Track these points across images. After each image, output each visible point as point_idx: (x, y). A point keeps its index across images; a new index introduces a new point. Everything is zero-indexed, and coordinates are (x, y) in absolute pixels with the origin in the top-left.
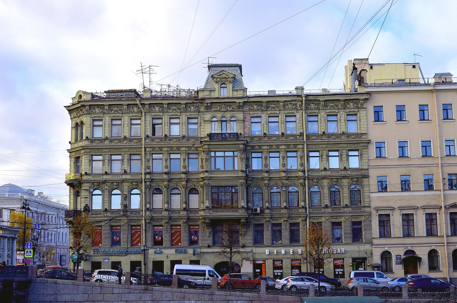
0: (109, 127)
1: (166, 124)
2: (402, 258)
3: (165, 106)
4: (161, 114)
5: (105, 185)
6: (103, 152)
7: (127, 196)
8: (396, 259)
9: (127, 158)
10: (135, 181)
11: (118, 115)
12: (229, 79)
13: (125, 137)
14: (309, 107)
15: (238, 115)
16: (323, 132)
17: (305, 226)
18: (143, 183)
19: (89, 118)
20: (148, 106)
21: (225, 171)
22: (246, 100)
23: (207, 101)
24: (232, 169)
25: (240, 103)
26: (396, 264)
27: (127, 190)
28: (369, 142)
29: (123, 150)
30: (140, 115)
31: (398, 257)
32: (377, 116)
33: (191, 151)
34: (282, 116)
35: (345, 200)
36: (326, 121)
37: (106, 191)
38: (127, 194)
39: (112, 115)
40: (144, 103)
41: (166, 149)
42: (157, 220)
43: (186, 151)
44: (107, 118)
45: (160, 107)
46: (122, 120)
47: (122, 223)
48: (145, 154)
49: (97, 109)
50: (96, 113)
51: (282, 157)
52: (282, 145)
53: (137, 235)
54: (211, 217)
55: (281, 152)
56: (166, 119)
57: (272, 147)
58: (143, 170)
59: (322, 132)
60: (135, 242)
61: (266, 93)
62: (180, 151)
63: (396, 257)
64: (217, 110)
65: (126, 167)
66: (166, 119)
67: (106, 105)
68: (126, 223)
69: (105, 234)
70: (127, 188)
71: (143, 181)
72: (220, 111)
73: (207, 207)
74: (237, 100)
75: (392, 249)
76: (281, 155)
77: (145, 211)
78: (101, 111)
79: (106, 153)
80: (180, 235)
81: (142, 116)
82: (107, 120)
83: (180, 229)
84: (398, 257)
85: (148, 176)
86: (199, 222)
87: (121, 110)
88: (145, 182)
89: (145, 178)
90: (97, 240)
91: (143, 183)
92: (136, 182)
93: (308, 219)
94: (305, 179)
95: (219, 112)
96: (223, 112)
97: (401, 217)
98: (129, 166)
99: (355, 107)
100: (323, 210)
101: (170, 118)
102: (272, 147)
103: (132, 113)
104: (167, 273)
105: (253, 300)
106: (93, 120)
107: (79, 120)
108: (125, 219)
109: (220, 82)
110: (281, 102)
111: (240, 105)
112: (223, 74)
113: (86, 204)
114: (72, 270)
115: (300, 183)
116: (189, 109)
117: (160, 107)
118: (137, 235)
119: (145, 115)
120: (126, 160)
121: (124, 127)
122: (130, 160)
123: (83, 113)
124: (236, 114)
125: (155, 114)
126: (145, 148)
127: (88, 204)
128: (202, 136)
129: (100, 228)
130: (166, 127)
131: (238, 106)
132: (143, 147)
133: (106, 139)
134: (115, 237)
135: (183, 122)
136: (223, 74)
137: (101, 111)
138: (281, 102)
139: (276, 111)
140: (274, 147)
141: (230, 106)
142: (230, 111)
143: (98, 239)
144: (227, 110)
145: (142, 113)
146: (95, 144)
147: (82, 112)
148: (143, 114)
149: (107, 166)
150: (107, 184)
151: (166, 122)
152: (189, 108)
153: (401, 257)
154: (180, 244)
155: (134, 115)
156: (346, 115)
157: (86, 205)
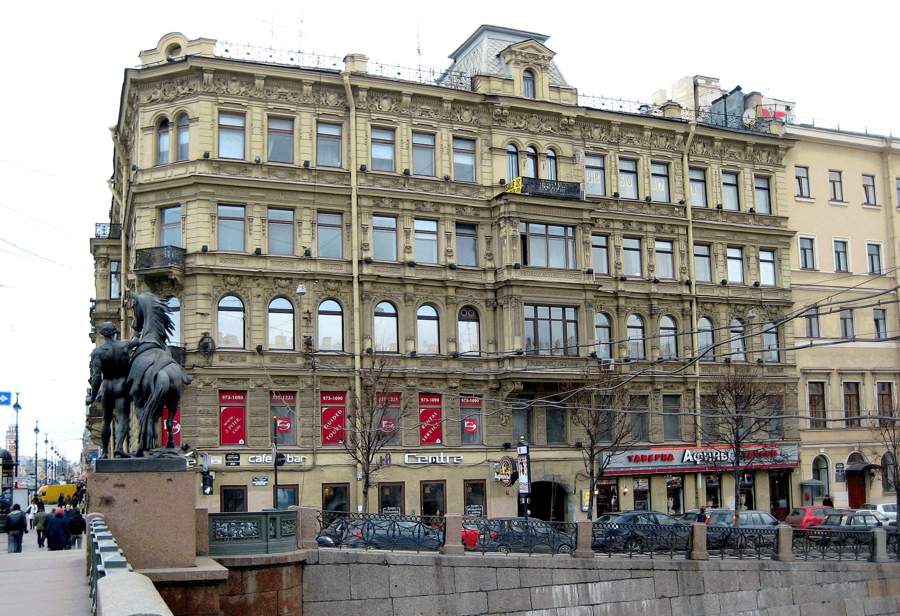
2: (845, 469)
3: (363, 94)
5: (255, 284)
6: (248, 199)
8: (837, 471)
9: (308, 218)
10: (334, 279)
11: (286, 106)
13: (307, 164)
14: (758, 157)
15: (561, 145)
16: (305, 161)
17: (692, 403)
18: (356, 285)
19: (209, 104)
21: (547, 270)
22: (582, 114)
23: (504, 103)
24: (544, 265)
25: (568, 118)
26: (837, 481)
28: (790, 235)
29: (302, 198)
30: (341, 113)
31: (839, 465)
33: (421, 211)
34: (445, 136)
36: (217, 126)
37: (255, 299)
39: (271, 105)
41: (407, 206)
42: (428, 382)
44: (304, 115)
45: (393, 102)
46: (248, 116)
48: (359, 214)
50: (380, 111)
51: (484, 238)
52: (650, 223)
53: (334, 418)
54: (529, 377)
55: (483, 227)
57: (382, 202)
58: (355, 253)
59: (303, 163)
60: (331, 435)
61: (635, 110)
63: (837, 468)
64: (519, 128)
67: (259, 78)
69: (255, 414)
71: (355, 281)
72: (527, 130)
73: (519, 353)
75: (831, 452)
76: (401, 225)
77: (361, 358)
78: (243, 89)
80: (439, 416)
82: (257, 116)
83: (440, 403)
84: (839, 465)
85: (367, 270)
86: (483, 389)
87: (294, 95)
88: (361, 283)
89: (360, 275)
90: (233, 429)
91: (356, 285)
92: (286, 279)
95: (522, 131)
96: (533, 133)
97: (842, 389)
99: (391, 111)
100: (249, 358)
102: (382, 202)
103: (458, 122)
104: (414, 512)
107: (171, 110)
109: (522, 64)
110: (306, 84)
111: (502, 114)
112: (532, 47)
113: (205, 331)
115: (487, 301)
116: (458, 116)
117: (393, 102)
118: (334, 418)
121: (252, 133)
123: (190, 90)
124: (519, 138)
125: (381, 116)
126: (358, 196)
127: (209, 331)
128: (487, 183)
131: (499, 115)
133: (258, 164)
134: (466, 423)
136: (532, 47)
138: (306, 84)
139: (430, 122)
140: (469, 210)
141: (185, 85)
142: (548, 133)
143: (235, 427)
145: (348, 109)
146: (274, 178)
147: (186, 89)
148: (353, 112)
150: (261, 281)
151: (405, 140)
153: (843, 468)
154: (438, 441)
155: (327, 111)
156: (266, 117)
157: (205, 334)
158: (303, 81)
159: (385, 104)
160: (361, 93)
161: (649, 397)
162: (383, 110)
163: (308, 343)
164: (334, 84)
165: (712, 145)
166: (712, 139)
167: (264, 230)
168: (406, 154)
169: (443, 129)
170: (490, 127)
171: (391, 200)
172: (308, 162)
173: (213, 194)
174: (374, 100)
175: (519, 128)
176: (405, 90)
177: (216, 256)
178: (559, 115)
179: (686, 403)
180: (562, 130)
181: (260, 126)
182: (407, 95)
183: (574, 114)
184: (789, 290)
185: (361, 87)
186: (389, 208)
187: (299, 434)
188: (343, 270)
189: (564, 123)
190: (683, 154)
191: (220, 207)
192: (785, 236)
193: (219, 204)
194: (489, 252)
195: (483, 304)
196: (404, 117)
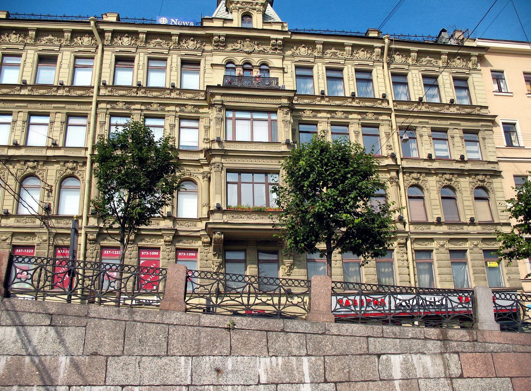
0: (32, 66)
1: (141, 67)
3: (108, 35)
4: (133, 50)
6: (14, 108)
7: (53, 188)
12: (257, 7)
20: (110, 34)
25: (277, 40)
27: (54, 178)
32: (103, 70)
33: (183, 112)
35: (467, 212)
38: (54, 185)
40: (27, 28)
43: (176, 112)
44: (29, 52)
47: (35, 241)
49: (15, 36)
51: (203, 127)
55: (321, 124)
56: (142, 59)
62: (165, 111)
65: (58, 136)
66: (142, 59)
68: (45, 241)
70: (54, 174)
74: (272, 34)
79: (20, 110)
81: (96, 52)
83: (158, 256)
93: (409, 243)
94: (398, 173)
96: (246, 52)
98: (62, 135)
101: (4, 55)
103: (80, 46)
105: (462, 352)
106: (76, 58)
108: (44, 231)
114: (196, 274)
119: (103, 51)
120: (57, 124)
121: (60, 68)
122: (66, 124)
124: (253, 58)
126: (98, 103)
129: (156, 253)
130: (141, 72)
132: (94, 100)
135: (140, 64)
137: (133, 42)
142: (259, 52)
144: (253, 51)
145: (97, 48)
149: (18, 133)
152: (186, 43)
155: (82, 49)
158: (64, 30)
159: (126, 40)
160: (106, 34)
161: (395, 251)
162: (125, 44)
163: (48, 209)
164: (357, 44)
165: (137, 38)
166: (136, 33)
167: (23, 129)
168: (353, 84)
169: (319, 63)
170: (211, 51)
171: (124, 103)
172: (422, 98)
173: (64, 108)
174: (118, 39)
175: (235, 50)
176: (173, 31)
177: (61, 150)
178: (269, 39)
179: (400, 255)
180: (222, 46)
181: (449, 83)
182: (176, 35)
183: (281, 37)
184: (496, 163)
185: (173, 33)
186: (341, 118)
187: (506, 278)
188: (82, 154)
189: (273, 43)
190: (383, 63)
191: (300, 126)
192: (466, 119)
193: (299, 124)
194: (206, 137)
195: (200, 177)
196: (142, 49)
